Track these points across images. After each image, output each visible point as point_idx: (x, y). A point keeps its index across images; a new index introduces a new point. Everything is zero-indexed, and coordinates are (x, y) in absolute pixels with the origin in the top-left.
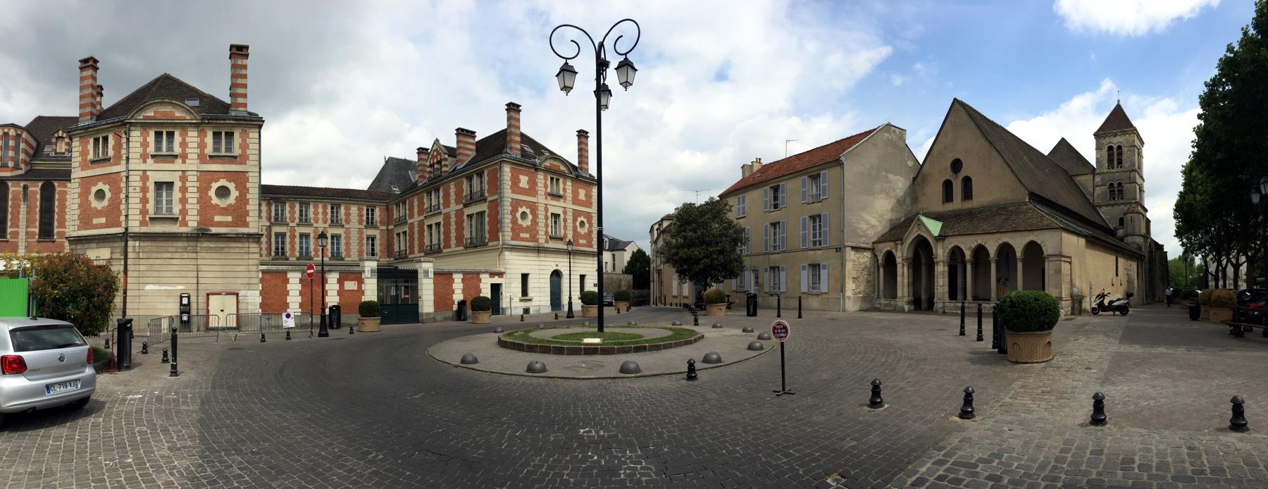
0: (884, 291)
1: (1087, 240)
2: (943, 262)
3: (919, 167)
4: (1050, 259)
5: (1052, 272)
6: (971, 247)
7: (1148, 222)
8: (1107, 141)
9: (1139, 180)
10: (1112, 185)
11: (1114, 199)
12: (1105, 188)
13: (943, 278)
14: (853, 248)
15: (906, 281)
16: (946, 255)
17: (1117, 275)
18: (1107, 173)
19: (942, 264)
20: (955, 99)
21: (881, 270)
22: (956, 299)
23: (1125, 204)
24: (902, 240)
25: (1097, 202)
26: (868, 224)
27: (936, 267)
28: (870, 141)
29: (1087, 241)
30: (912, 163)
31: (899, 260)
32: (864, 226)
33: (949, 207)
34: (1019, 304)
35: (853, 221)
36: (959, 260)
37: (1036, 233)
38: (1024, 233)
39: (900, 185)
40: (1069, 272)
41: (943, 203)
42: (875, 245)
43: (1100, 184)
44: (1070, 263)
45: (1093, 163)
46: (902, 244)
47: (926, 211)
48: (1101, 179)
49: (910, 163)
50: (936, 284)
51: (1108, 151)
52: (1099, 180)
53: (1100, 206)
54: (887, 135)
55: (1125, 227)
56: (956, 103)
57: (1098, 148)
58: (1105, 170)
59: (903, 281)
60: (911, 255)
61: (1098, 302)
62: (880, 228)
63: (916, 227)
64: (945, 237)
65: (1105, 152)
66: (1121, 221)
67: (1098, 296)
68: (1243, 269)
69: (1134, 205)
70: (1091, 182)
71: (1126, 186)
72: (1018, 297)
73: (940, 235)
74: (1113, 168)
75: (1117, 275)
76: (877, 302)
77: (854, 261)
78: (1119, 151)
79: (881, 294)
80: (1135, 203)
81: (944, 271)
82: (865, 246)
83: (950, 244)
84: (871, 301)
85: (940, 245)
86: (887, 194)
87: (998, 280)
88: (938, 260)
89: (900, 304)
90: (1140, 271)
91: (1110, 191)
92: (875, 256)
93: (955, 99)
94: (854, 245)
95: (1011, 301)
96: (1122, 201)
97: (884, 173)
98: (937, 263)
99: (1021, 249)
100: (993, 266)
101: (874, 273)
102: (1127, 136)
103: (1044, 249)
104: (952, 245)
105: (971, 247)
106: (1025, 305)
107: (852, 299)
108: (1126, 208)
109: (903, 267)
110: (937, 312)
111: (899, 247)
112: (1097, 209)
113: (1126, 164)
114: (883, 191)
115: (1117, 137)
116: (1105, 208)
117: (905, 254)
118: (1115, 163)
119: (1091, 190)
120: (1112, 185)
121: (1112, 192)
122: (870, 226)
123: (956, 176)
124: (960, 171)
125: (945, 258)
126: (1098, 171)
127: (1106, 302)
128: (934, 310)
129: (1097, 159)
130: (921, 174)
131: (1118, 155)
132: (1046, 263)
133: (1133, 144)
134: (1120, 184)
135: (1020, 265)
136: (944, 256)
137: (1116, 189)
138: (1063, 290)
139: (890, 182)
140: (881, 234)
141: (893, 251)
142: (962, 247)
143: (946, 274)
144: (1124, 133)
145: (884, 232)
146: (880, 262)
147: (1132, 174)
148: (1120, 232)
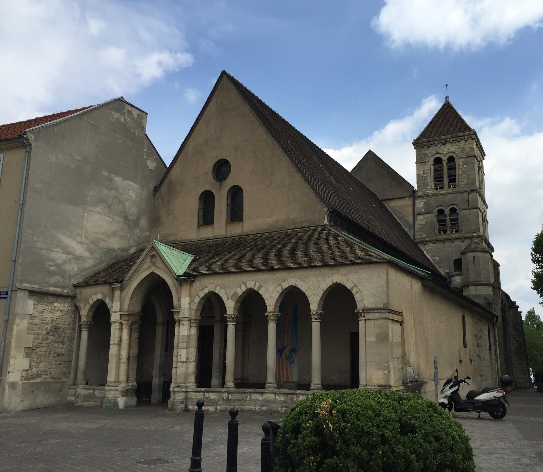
0: (85, 373)
1: (423, 285)
2: (189, 320)
3: (166, 170)
4: (368, 316)
5: (371, 339)
6: (236, 293)
7: (496, 266)
8: (432, 152)
9: (481, 205)
10: (441, 212)
11: (445, 232)
12: (432, 217)
13: (188, 348)
14: (32, 293)
15: (124, 353)
16: (194, 307)
17: (465, 346)
18: (434, 195)
19: (186, 323)
20: (224, 73)
21: (85, 334)
22: (209, 386)
23: (463, 239)
24: (121, 282)
25: (419, 236)
26: (68, 253)
27: (177, 328)
28: (85, 118)
29: (425, 287)
30: (154, 164)
31: (115, 317)
32: (59, 256)
33: (208, 233)
34: (346, 443)
35: (38, 245)
36: (218, 317)
37: (343, 270)
38: (324, 271)
39: (132, 195)
40: (399, 340)
41: (199, 226)
42: (78, 290)
43: (423, 210)
44: (401, 323)
45: (413, 182)
46: (122, 289)
47: (172, 238)
48: (425, 204)
49: (151, 165)
50: (175, 359)
51: (434, 165)
52: (422, 205)
53: (424, 243)
54: (117, 115)
55: (464, 271)
56: (225, 78)
57: (420, 161)
58: (431, 192)
59: (119, 355)
60: (137, 308)
61: (449, 392)
62: (90, 263)
63: (148, 260)
64: (195, 276)
65: (430, 166)
66: (458, 264)
67: (448, 382)
68: (39, 380)
69: (476, 240)
70: (410, 210)
71: (463, 214)
72: (343, 413)
73: (186, 274)
74: (442, 188)
75: (465, 346)
76: (71, 392)
77: (32, 316)
78: (451, 164)
79: (80, 376)
80: (477, 237)
81: (189, 336)
82: (59, 290)
83: (203, 289)
84: (60, 390)
85: (185, 290)
86: (109, 207)
87: (279, 352)
88: (181, 315)
89: (110, 395)
90: (492, 341)
91: (439, 222)
92: (77, 309)
93: (224, 73)
94: (35, 287)
95: (318, 431)
96: (457, 235)
97: (105, 173)
98: (179, 321)
99: (319, 298)
100: (272, 327)
101: (71, 340)
102: (462, 143)
103: (357, 297)
104: (206, 291)
105: (236, 293)
106: (371, 448)
107: (19, 389)
108: (463, 245)
109: (121, 329)
110: (172, 409)
111: (117, 293)
112: (421, 247)
113: (462, 182)
114: (101, 201)
115: (448, 145)
116: (431, 245)
117: (126, 307)
118: (446, 181)
119: (411, 220)
120: (441, 212)
121: (442, 223)
122: (70, 257)
123: (221, 186)
124: (225, 179)
125: (193, 313)
126: (420, 193)
127: (463, 394)
128: (169, 406)
129: (418, 176)
130: (166, 182)
131: (449, 169)
132: (361, 324)
133: (472, 154)
134: (453, 211)
135: (316, 326)
136: (191, 309)
137: (448, 218)
138: (392, 372)
139: (116, 189)
140: (90, 272)
141: (107, 301)
142: (222, 294)
143: (194, 342)
144: (458, 139)
145: (96, 269)
146: (84, 319)
147: (471, 196)
148: (457, 280)
